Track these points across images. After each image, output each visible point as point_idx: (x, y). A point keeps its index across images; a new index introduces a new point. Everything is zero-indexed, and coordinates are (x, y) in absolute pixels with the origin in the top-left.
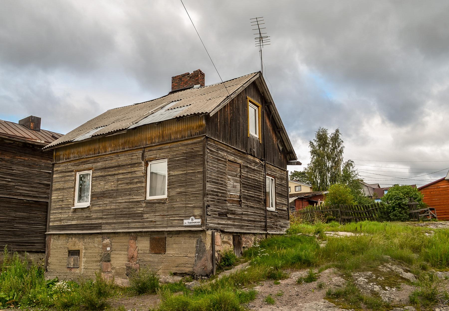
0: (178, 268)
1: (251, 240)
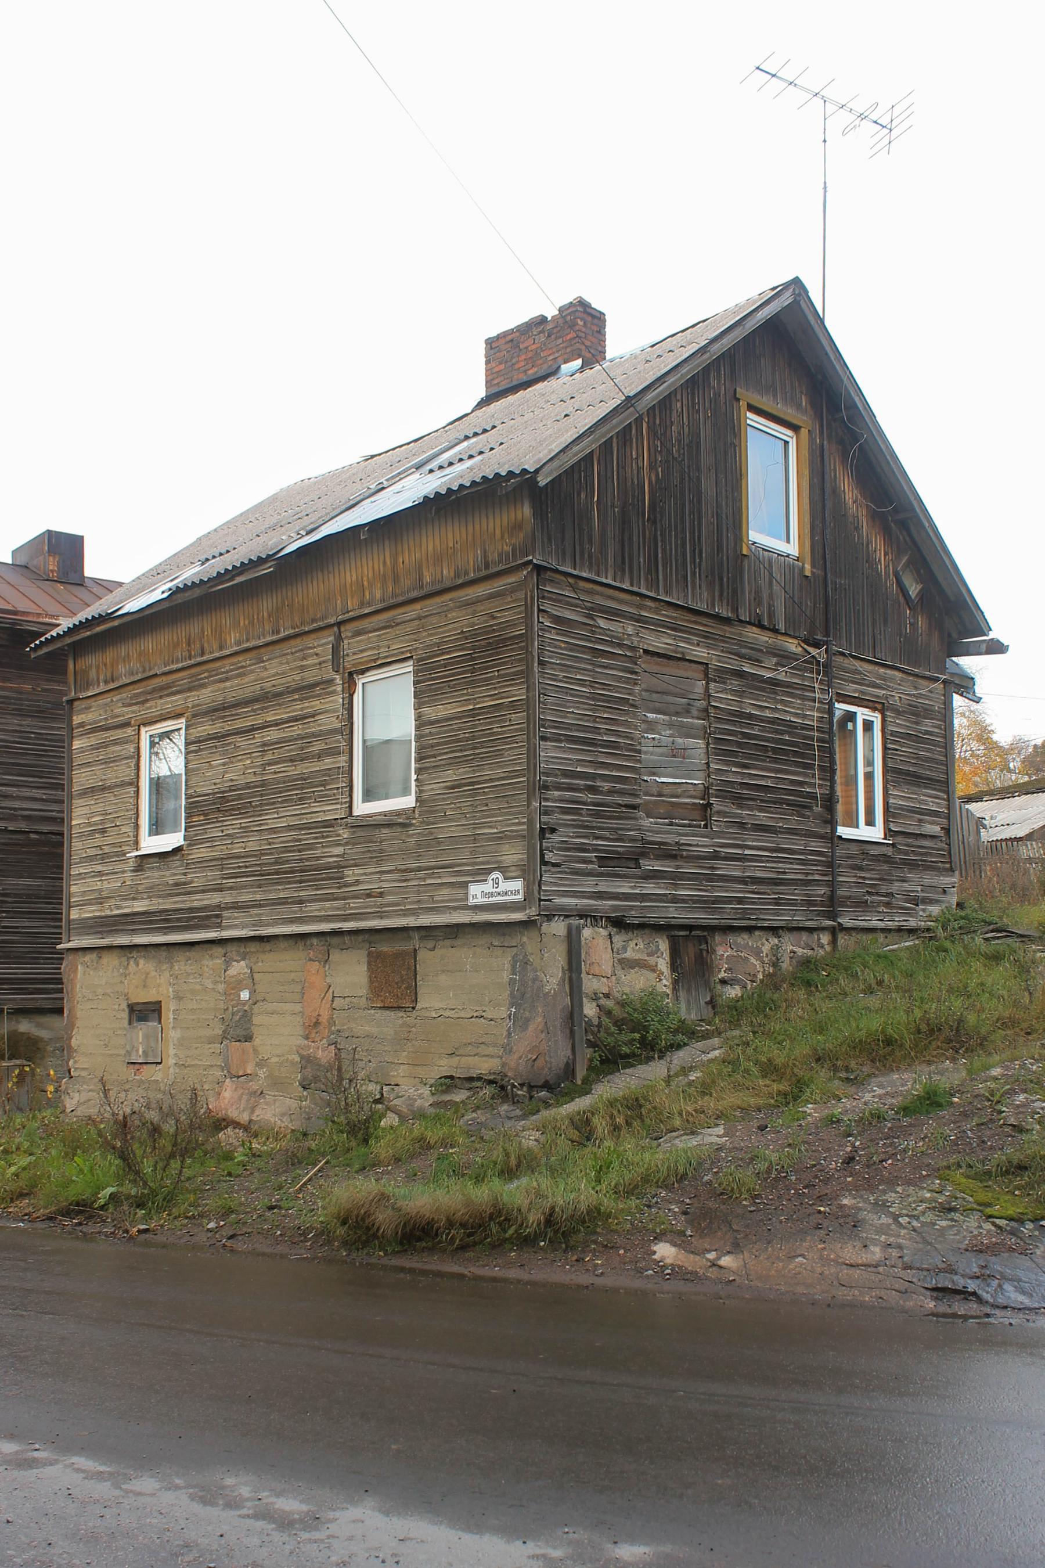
0: (456, 1060)
1: (757, 953)
